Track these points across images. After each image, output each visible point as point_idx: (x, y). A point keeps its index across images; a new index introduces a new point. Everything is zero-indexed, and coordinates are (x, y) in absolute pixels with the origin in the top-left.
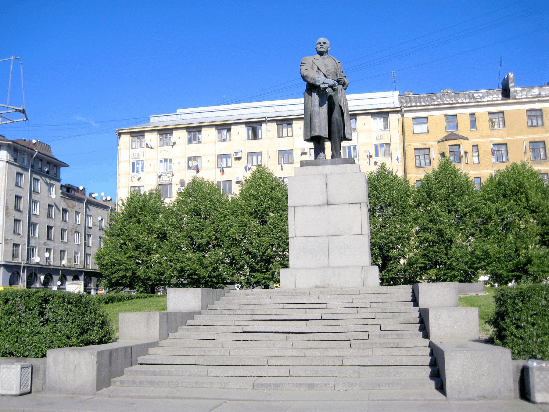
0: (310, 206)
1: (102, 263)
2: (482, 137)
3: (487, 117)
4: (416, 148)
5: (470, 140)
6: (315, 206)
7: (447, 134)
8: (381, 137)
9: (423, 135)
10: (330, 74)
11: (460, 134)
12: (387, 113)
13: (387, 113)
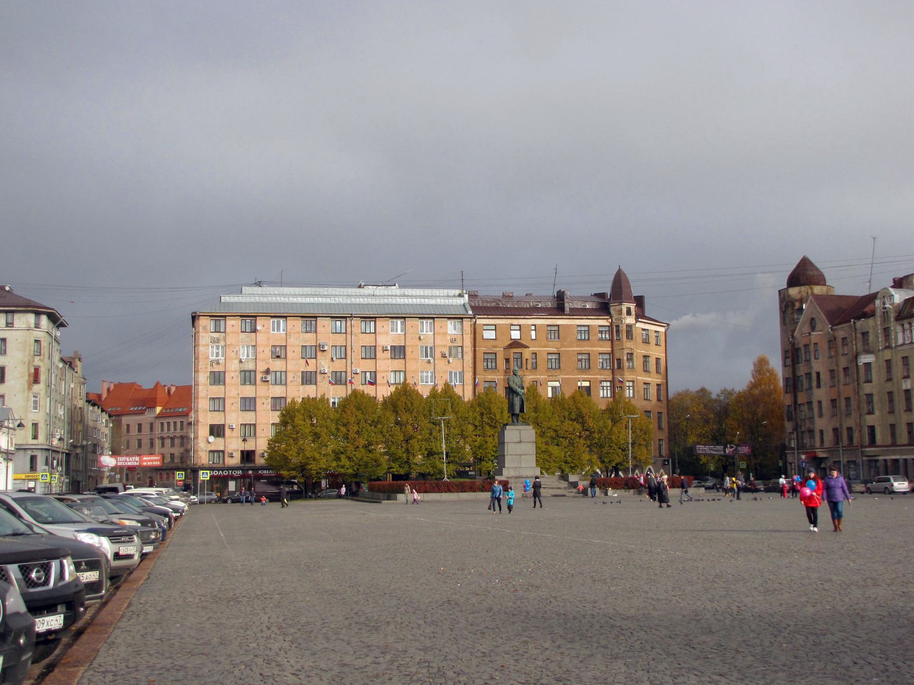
5: (530, 349)
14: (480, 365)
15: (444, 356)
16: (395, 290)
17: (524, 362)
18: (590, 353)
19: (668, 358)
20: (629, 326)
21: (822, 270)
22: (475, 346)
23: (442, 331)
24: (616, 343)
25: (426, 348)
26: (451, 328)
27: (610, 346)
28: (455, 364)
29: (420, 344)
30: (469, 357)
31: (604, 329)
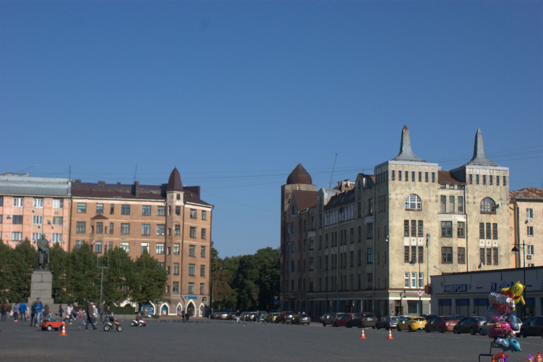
1: (67, 301)
2: (116, 218)
3: (157, 208)
5: (109, 220)
9: (469, 243)
12: (63, 198)
14: (74, 230)
15: (49, 223)
16: (25, 178)
17: (104, 228)
18: (151, 224)
19: (212, 229)
20: (178, 208)
21: (310, 174)
22: (71, 216)
23: (49, 206)
24: (168, 218)
25: (38, 217)
26: (56, 203)
27: (165, 220)
28: (57, 229)
29: (33, 214)
30: (66, 224)
31: (161, 208)
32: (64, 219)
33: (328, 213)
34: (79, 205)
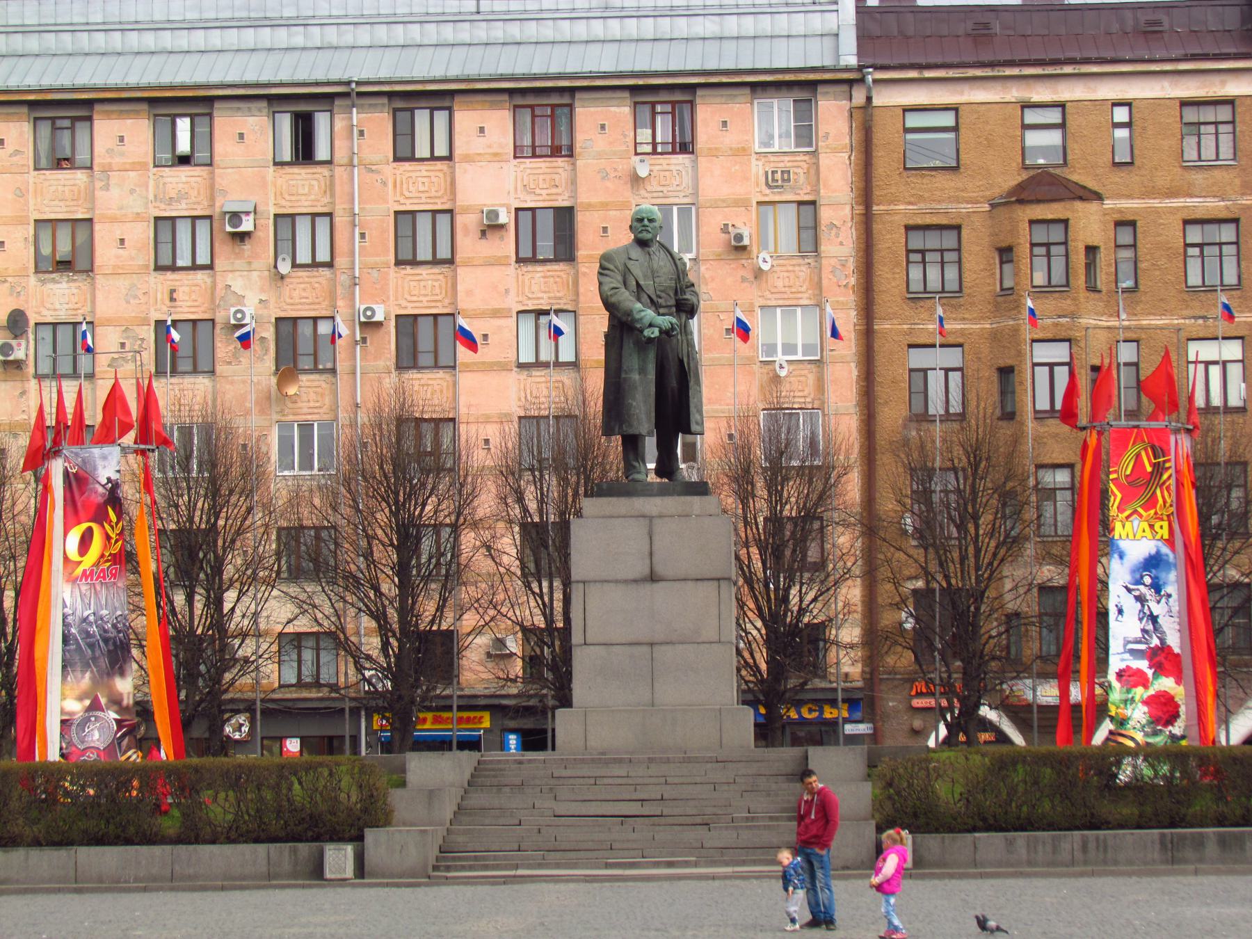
0: (617, 581)
3: (1171, 118)
4: (911, 222)
5: (1109, 204)
6: (626, 582)
7: (1025, 175)
8: (786, 176)
10: (663, 295)
11: (1075, 177)
13: (812, 85)
32: (826, 215)
33: (737, 435)
34: (913, 121)
